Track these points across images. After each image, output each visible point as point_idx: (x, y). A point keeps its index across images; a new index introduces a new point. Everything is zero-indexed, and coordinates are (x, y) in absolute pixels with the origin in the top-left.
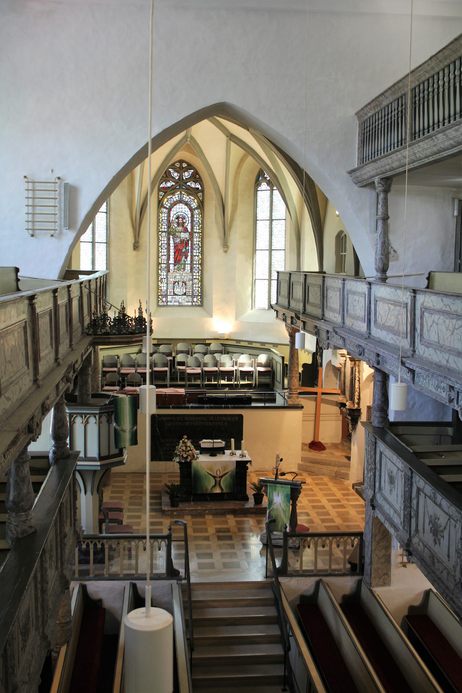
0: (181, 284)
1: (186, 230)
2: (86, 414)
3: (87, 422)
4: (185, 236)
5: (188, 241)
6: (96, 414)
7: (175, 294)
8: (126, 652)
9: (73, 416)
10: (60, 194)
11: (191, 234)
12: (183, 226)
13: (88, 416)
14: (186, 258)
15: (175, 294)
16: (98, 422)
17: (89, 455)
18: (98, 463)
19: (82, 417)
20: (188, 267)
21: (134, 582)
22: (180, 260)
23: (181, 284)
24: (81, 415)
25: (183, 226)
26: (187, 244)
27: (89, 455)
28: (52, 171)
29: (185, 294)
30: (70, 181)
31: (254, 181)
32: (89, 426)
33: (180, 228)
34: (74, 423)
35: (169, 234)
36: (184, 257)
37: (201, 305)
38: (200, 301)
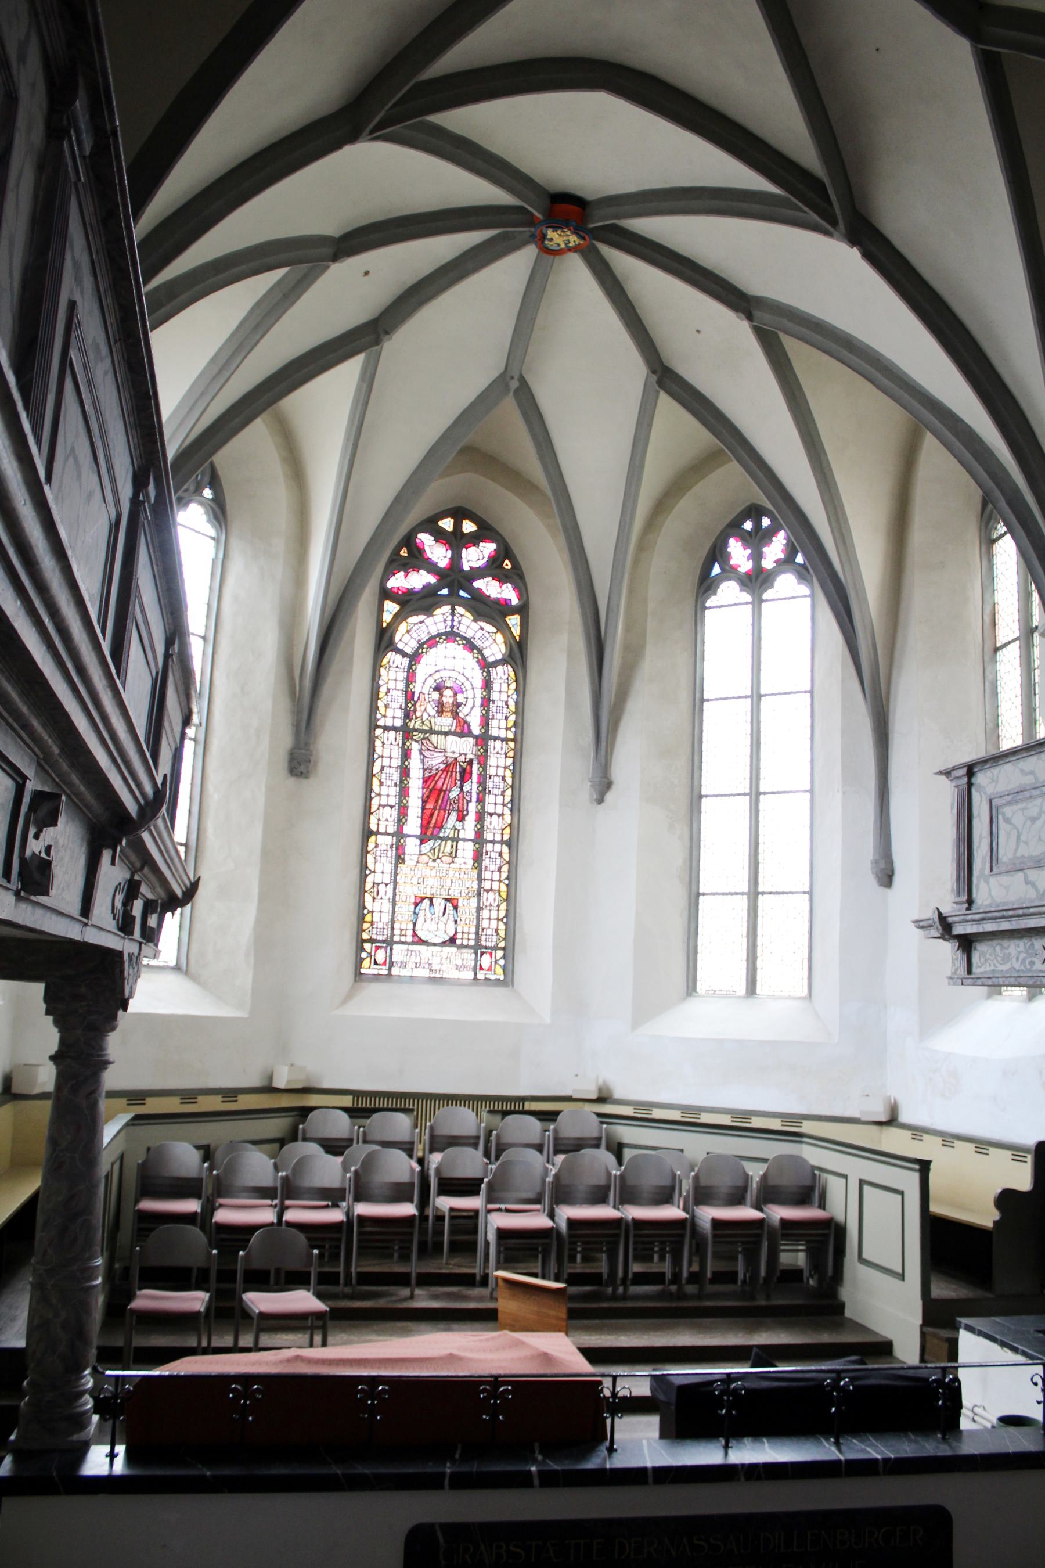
4: (462, 747)
11: (483, 740)
14: (461, 818)
20: (467, 850)
22: (440, 826)
25: (455, 715)
26: (465, 775)
29: (452, 941)
33: (446, 722)
35: (407, 733)
36: (454, 816)
37: (507, 981)
38: (504, 968)
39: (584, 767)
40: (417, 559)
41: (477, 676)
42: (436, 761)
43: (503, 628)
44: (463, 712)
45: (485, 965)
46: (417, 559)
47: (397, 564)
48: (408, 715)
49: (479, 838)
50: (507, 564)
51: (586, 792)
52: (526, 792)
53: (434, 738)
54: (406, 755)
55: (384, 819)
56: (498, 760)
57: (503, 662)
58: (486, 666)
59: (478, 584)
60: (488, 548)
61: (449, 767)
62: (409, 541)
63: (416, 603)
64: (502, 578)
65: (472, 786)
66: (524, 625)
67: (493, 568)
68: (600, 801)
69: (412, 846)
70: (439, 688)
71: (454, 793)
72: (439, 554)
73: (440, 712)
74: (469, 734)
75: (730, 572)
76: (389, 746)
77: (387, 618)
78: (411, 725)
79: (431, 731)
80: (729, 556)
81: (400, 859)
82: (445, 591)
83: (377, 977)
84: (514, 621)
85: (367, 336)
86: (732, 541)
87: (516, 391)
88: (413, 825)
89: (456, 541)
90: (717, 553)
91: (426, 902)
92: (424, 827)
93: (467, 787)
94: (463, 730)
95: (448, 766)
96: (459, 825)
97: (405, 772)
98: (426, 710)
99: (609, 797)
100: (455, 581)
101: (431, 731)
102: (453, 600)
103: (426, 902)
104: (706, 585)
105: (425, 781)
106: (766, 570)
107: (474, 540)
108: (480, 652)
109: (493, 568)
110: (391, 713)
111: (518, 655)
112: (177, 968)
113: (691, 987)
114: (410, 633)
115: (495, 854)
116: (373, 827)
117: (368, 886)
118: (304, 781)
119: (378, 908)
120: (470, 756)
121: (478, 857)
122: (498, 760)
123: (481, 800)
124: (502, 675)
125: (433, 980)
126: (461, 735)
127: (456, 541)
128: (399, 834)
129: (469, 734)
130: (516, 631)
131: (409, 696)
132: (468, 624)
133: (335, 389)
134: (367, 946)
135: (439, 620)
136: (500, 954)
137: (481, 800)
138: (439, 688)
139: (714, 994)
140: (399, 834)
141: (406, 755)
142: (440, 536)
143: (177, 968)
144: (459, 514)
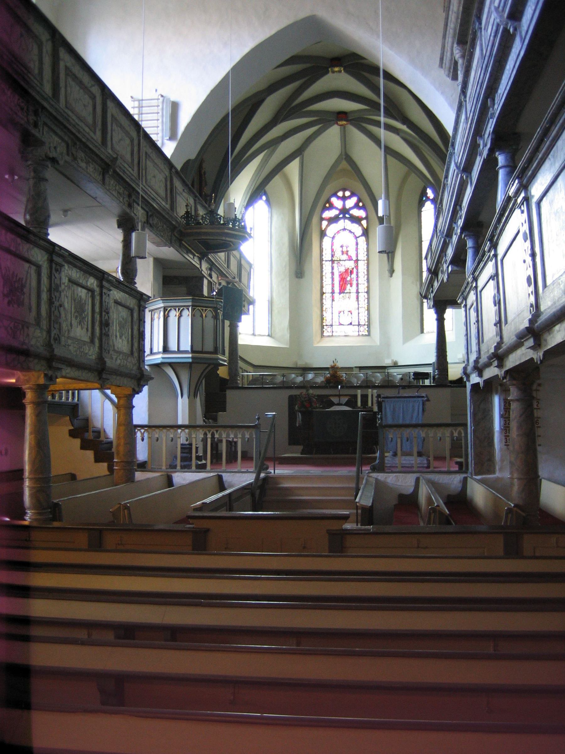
0: (346, 312)
1: (350, 259)
2: (179, 307)
3: (180, 316)
4: (350, 265)
5: (353, 269)
6: (189, 306)
7: (340, 324)
8: (69, 182)
9: (167, 310)
10: (163, 109)
11: (357, 261)
12: (347, 254)
13: (182, 308)
14: (351, 286)
15: (340, 324)
16: (190, 314)
17: (182, 349)
18: (190, 355)
19: (175, 310)
20: (354, 295)
21: (220, 474)
22: (345, 289)
23: (346, 312)
24: (175, 307)
25: (347, 254)
26: (352, 272)
27: (182, 349)
28: (156, 90)
29: (351, 324)
30: (173, 99)
31: (417, 201)
32: (182, 319)
33: (345, 257)
34: (168, 316)
35: (333, 261)
36: (349, 285)
37: (369, 335)
38: (368, 331)
39: (386, 267)
40: (332, 207)
41: (354, 241)
42: (342, 269)
43: (361, 225)
44: (349, 254)
45: (362, 330)
46: (332, 207)
47: (324, 209)
48: (333, 256)
49: (358, 292)
50: (361, 204)
51: (387, 274)
52: (370, 276)
53: (341, 262)
54: (333, 268)
55: (327, 289)
56: (362, 266)
57: (362, 236)
58: (356, 238)
59: (352, 212)
60: (354, 200)
61: (347, 270)
62: (328, 201)
63: (333, 220)
64: (359, 208)
65: (354, 276)
66: (367, 223)
67: (356, 206)
68: (391, 276)
69: (336, 295)
70: (342, 247)
71: (349, 279)
72: (338, 203)
73: (343, 253)
74: (352, 260)
75: (428, 199)
76: (327, 267)
77: (324, 227)
78: (334, 259)
79: (340, 260)
80: (427, 193)
81: (333, 300)
82: (341, 216)
83: (329, 336)
84: (364, 223)
85: (299, 152)
86: (428, 189)
87: (345, 159)
88: (337, 289)
89: (344, 198)
90: (424, 193)
91: (342, 312)
92: (340, 290)
93: (352, 276)
94: (350, 259)
95: (346, 270)
96: (351, 288)
97: (333, 274)
98: (338, 255)
99: (394, 275)
100: (344, 211)
101: (340, 260)
102: (344, 217)
103: (342, 312)
104: (421, 204)
105: (340, 275)
106: (434, 198)
107: (349, 197)
108: (354, 233)
109: (356, 206)
110: (327, 256)
111: (366, 233)
112: (269, 335)
113: (422, 331)
114: (332, 230)
115: (363, 296)
116: (324, 291)
117: (324, 309)
118: (301, 280)
119: (327, 316)
120: (353, 267)
121: (357, 298)
122: (362, 266)
123: (357, 280)
124: (362, 240)
125: (346, 336)
126: (350, 260)
127: (344, 198)
128: (333, 292)
129: (352, 260)
130: (365, 226)
131: (332, 250)
132: (348, 224)
133: (293, 168)
134: (325, 327)
135: (342, 224)
136: (366, 326)
137: (357, 280)
138: (342, 247)
139: (429, 333)
140: (333, 292)
141: (333, 268)
142: (339, 198)
143: (269, 335)
144: (344, 190)
